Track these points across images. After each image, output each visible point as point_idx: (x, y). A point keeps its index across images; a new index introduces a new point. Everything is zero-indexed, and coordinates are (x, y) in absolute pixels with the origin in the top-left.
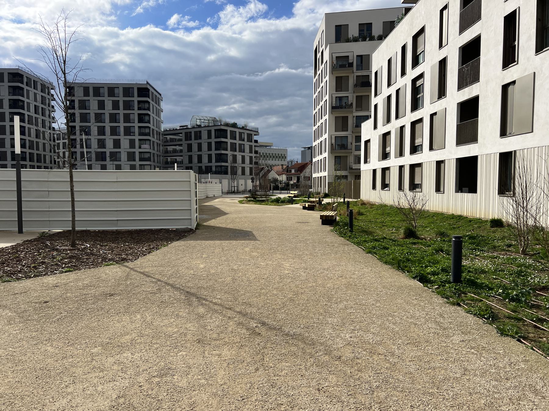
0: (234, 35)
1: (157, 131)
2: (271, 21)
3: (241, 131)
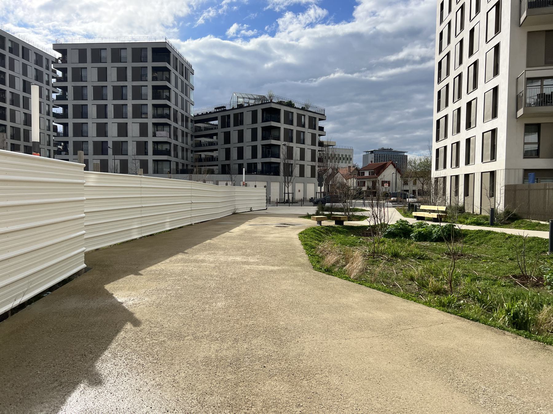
0: (291, 42)
1: (182, 115)
2: (330, 26)
3: (301, 112)
